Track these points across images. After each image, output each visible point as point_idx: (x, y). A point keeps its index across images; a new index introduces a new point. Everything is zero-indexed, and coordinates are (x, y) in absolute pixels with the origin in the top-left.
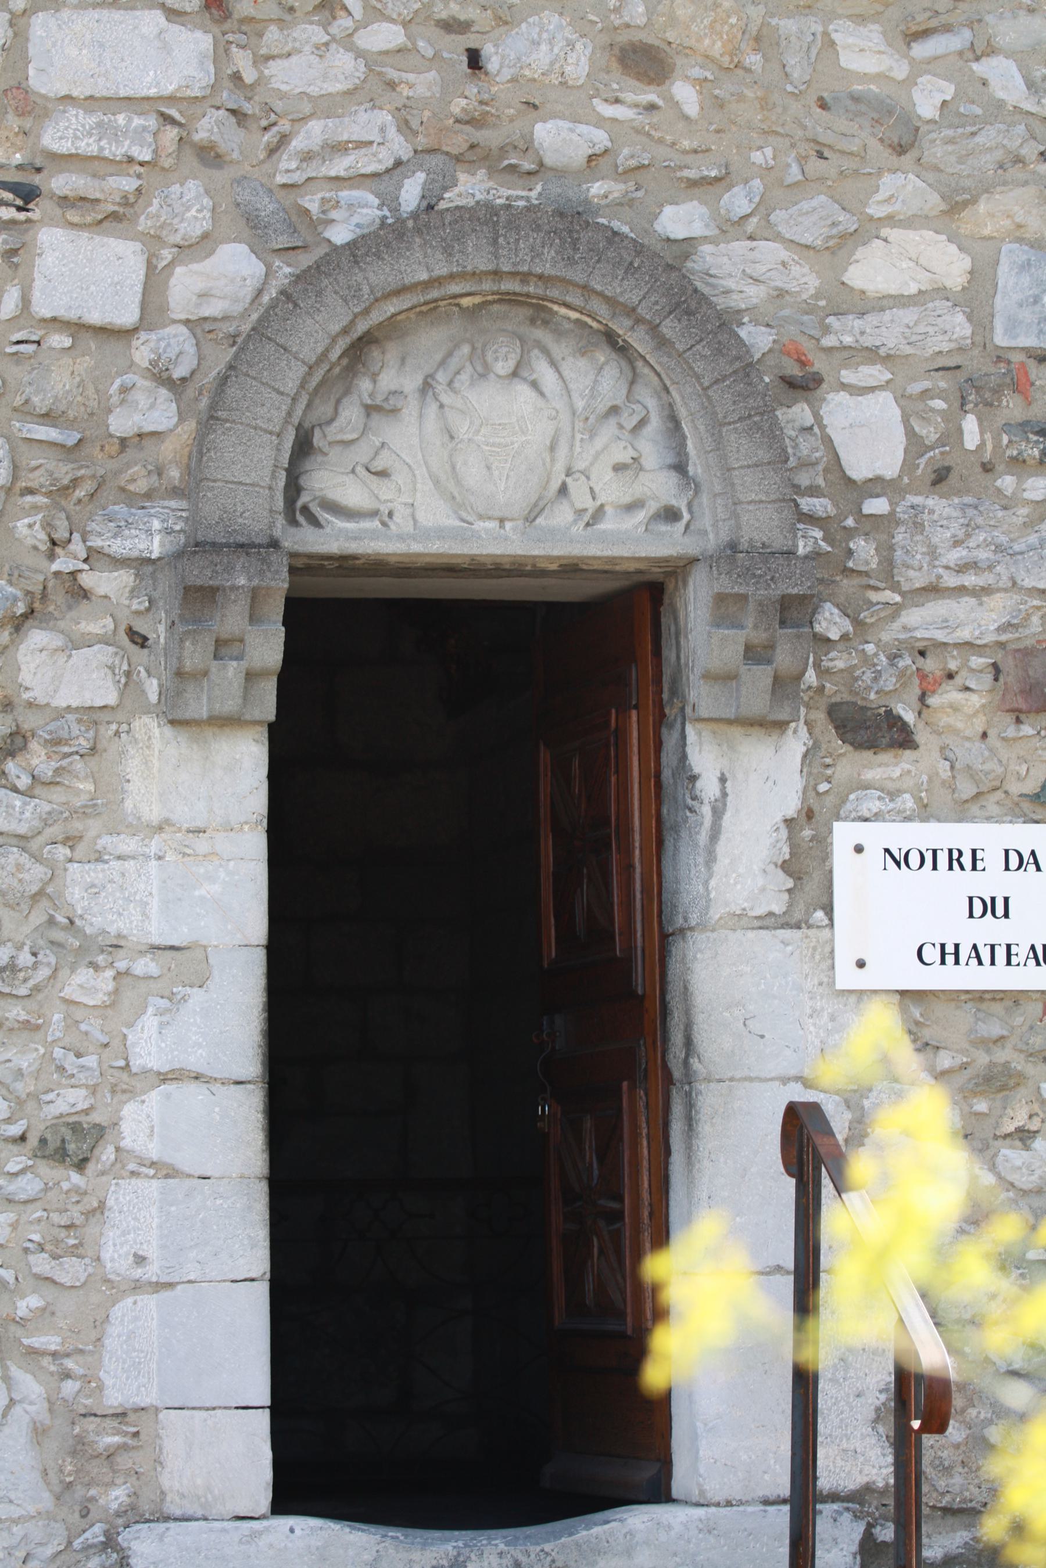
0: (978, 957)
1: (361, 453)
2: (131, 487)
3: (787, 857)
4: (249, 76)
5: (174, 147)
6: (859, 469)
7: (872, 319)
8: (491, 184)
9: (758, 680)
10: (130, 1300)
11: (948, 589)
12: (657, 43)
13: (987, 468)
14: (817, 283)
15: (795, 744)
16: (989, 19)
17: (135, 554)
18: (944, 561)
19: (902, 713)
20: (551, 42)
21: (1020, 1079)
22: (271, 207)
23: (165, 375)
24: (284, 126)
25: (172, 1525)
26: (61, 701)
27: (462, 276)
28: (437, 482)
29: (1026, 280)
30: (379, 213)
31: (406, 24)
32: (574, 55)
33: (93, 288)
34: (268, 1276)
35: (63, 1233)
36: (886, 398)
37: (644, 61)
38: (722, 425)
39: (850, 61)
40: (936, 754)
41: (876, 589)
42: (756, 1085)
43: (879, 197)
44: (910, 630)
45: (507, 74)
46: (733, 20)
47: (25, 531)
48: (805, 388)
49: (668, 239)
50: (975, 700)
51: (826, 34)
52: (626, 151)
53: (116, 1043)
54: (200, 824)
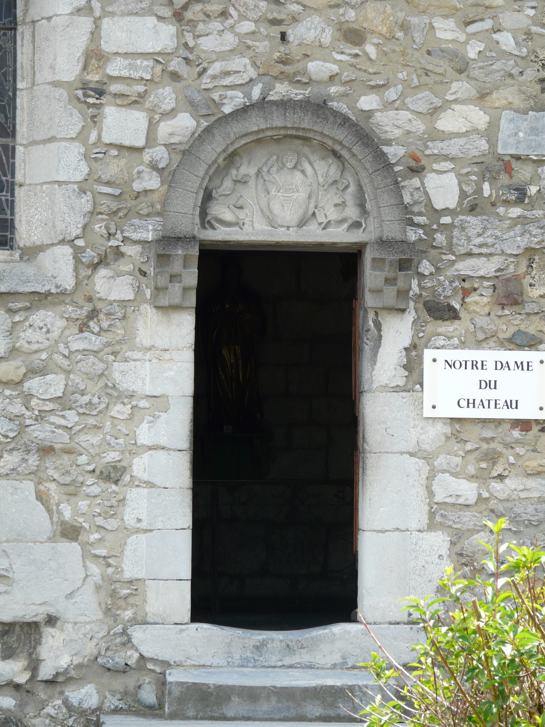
0: (483, 405)
1: (232, 200)
2: (141, 212)
3: (405, 363)
4: (191, 44)
5: (160, 73)
6: (439, 205)
7: (446, 143)
8: (289, 88)
9: (390, 292)
10: (135, 536)
11: (475, 254)
12: (360, 28)
13: (493, 204)
14: (424, 128)
15: (410, 317)
16: (501, 15)
17: (142, 239)
18: (473, 243)
19: (454, 305)
20: (315, 28)
21: (500, 455)
22: (199, 98)
23: (155, 167)
24: (205, 65)
25: (149, 626)
26: (112, 298)
27: (272, 128)
28: (262, 211)
29: (512, 126)
30: (243, 100)
31: (256, 22)
32: (325, 34)
33: (126, 131)
34: (191, 527)
35: (109, 509)
36: (452, 175)
37: (354, 36)
38: (377, 189)
39: (440, 34)
40: (469, 323)
41: (445, 254)
42: (390, 455)
43: (451, 92)
44: (459, 271)
45: (297, 42)
46: (391, 18)
47: (98, 230)
48: (417, 172)
49: (362, 110)
50: (485, 300)
51: (430, 23)
52: (345, 74)
53: (131, 434)
54: (166, 348)
